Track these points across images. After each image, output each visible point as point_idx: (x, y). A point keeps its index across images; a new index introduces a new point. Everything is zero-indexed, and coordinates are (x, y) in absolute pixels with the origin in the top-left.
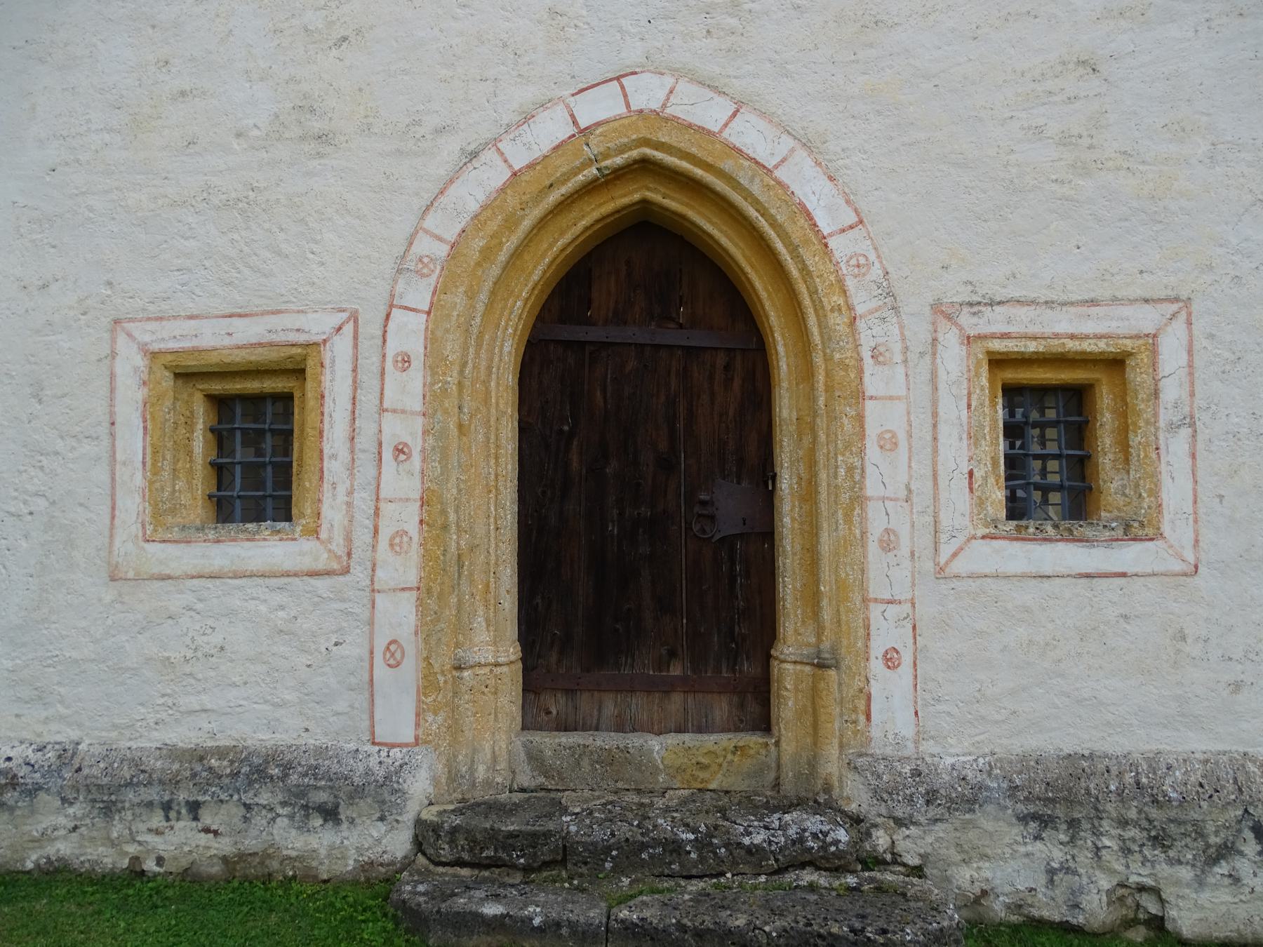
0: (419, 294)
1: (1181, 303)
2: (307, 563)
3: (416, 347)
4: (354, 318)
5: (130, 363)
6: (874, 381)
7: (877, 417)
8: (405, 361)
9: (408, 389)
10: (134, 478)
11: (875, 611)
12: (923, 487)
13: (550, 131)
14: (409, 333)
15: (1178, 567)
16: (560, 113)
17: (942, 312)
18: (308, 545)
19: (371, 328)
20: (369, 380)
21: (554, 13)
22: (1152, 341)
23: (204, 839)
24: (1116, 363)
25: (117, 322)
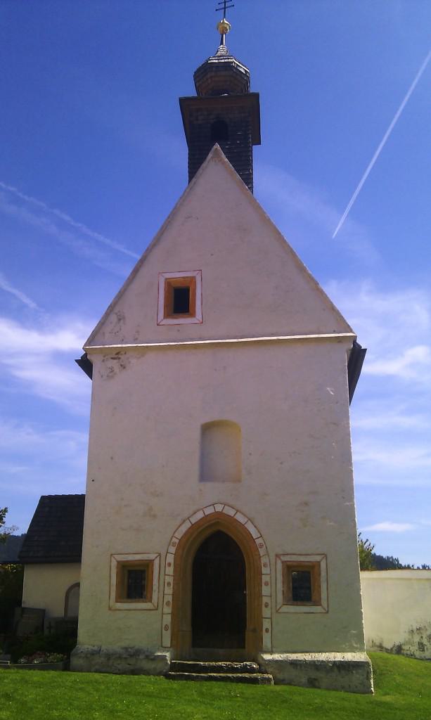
0: (173, 550)
1: (325, 556)
2: (149, 608)
3: (172, 561)
4: (160, 555)
5: (114, 563)
6: (264, 570)
7: (265, 578)
8: (169, 564)
9: (170, 570)
10: (114, 588)
11: (246, 525)
12: (274, 594)
13: (200, 515)
14: (171, 559)
15: (324, 611)
16: (201, 512)
17: (277, 556)
18: (150, 604)
19: (163, 558)
20: (273, 581)
21: (124, 368)
22: (319, 563)
23: (128, 666)
24: (313, 567)
25: (112, 555)
